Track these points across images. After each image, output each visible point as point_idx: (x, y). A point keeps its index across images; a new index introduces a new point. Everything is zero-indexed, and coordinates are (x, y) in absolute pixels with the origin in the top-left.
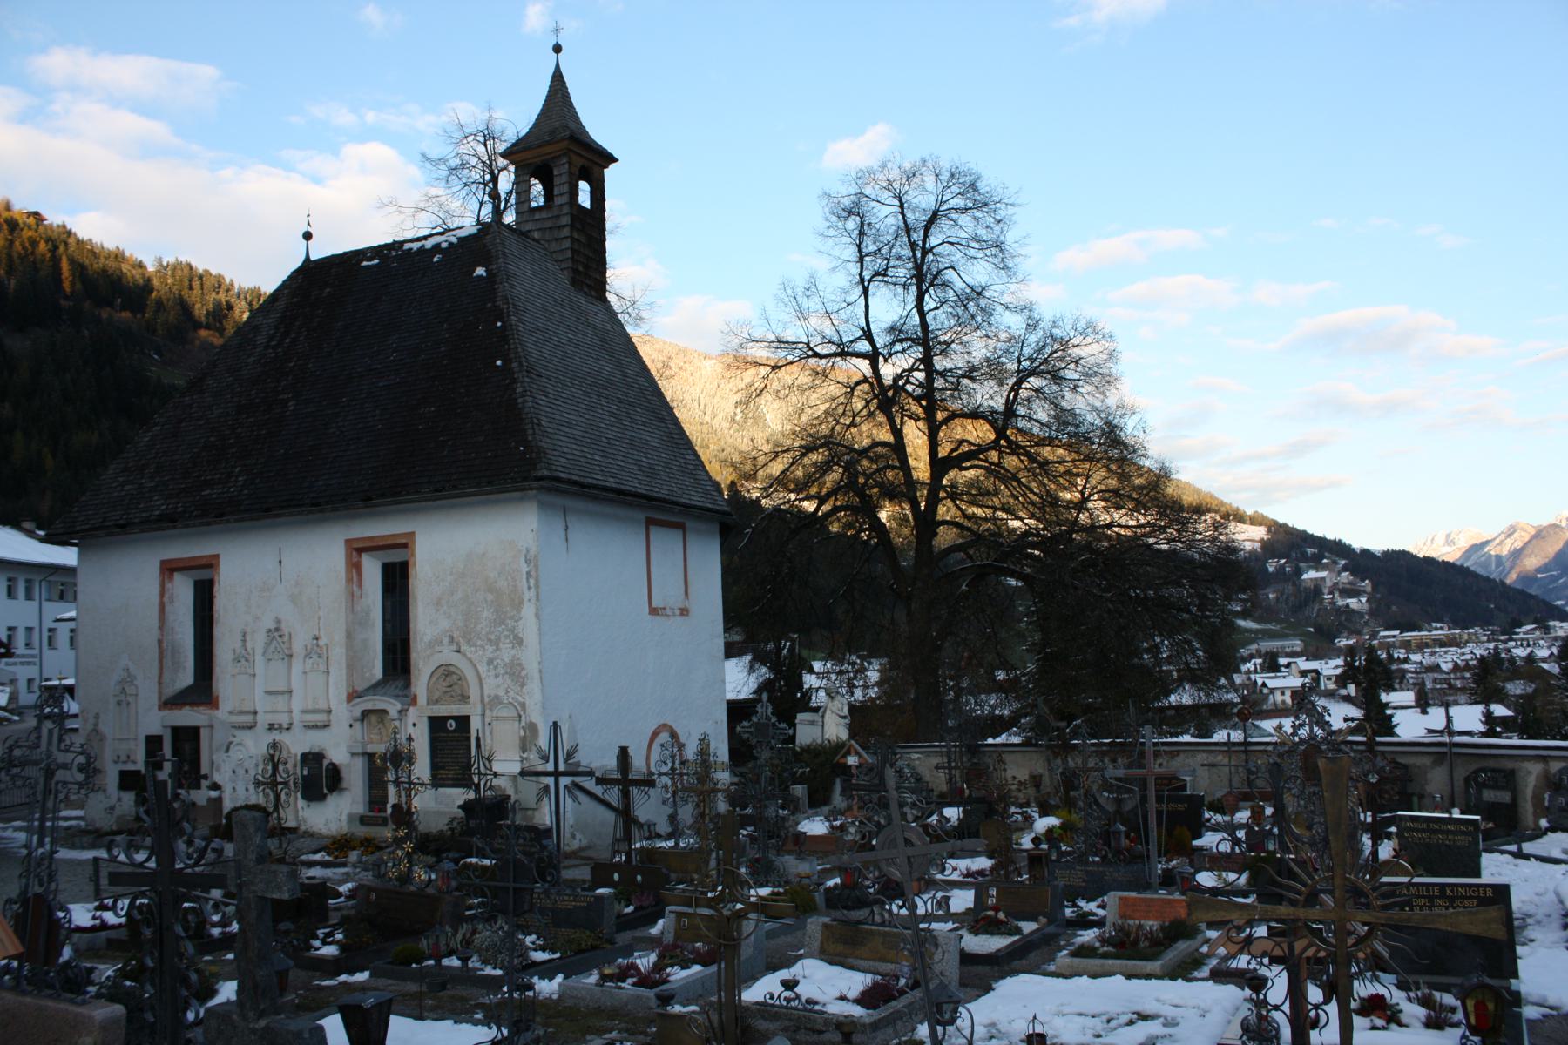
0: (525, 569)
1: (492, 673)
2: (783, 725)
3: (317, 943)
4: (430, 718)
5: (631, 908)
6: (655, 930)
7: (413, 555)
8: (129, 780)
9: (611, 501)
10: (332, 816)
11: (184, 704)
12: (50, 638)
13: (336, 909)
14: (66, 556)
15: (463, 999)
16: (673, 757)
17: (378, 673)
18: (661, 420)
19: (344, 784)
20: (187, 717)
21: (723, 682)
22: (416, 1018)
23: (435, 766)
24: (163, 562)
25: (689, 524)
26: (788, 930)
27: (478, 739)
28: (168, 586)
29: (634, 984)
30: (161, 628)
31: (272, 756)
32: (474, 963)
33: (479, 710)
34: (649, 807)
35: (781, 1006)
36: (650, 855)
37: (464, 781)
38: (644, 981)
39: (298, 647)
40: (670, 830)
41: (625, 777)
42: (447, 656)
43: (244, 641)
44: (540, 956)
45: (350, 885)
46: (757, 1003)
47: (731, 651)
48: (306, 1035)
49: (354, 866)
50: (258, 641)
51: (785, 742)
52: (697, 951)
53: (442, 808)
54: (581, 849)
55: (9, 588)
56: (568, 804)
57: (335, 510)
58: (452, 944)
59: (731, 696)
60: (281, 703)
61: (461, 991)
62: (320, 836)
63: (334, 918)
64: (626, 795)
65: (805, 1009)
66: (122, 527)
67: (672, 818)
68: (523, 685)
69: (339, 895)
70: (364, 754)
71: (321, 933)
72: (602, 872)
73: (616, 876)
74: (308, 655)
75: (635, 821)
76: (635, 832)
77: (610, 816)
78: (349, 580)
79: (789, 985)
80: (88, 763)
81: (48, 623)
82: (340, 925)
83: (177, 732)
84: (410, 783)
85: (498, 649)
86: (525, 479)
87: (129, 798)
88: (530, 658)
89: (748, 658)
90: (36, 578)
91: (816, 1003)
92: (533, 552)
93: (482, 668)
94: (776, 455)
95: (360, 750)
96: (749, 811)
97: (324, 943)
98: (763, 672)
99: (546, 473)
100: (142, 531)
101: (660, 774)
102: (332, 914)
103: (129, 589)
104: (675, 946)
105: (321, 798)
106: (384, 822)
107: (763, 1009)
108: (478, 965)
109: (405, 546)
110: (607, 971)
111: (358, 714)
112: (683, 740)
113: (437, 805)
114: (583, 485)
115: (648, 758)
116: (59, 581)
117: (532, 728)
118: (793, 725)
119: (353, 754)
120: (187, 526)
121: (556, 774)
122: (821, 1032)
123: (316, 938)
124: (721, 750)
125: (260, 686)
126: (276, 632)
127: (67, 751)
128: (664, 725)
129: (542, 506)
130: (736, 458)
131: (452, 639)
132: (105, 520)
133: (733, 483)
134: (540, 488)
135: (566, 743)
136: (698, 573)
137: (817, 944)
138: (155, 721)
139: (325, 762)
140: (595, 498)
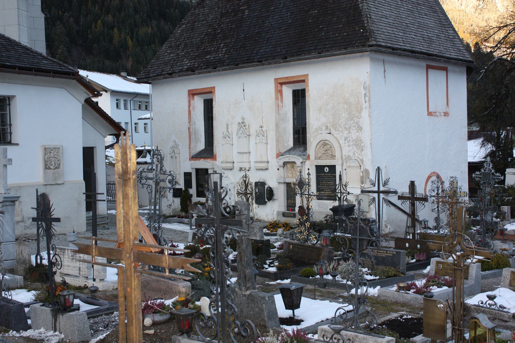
0: (363, 92)
1: (347, 144)
2: (498, 174)
3: (266, 266)
4: (316, 166)
5: (414, 260)
6: (425, 271)
7: (307, 86)
8: (177, 193)
9: (408, 56)
10: (269, 212)
11: (201, 158)
12: (135, 127)
13: (273, 253)
14: (144, 88)
15: (333, 293)
16: (438, 188)
17: (291, 144)
18: (435, 12)
19: (275, 197)
20: (202, 164)
21: (467, 151)
22: (312, 299)
23: (318, 190)
24: (189, 91)
25: (450, 68)
26: (494, 276)
27: (340, 176)
28: (192, 102)
29: (414, 293)
30: (189, 122)
31: (245, 181)
32: (338, 278)
33: (340, 162)
34: (425, 212)
35: (487, 308)
36: (425, 237)
37: (333, 198)
38: (419, 291)
39: (253, 131)
40: (435, 224)
41: (413, 197)
42: (325, 136)
43: (228, 128)
44: (369, 277)
45: (279, 243)
46: (475, 305)
47: (471, 136)
48: (267, 299)
49: (280, 236)
50: (234, 129)
51: (499, 183)
52: (446, 280)
53: (322, 210)
54: (390, 233)
55: (117, 104)
56: (385, 208)
57: (270, 64)
58: (328, 269)
59: (471, 160)
60: (245, 157)
61: (332, 290)
62: (264, 222)
63: (273, 257)
64: (413, 205)
65: (499, 310)
66: (170, 74)
67: (437, 219)
68: (362, 150)
69: (275, 247)
70: (284, 183)
71: (268, 262)
72: (400, 242)
73: (407, 245)
74: (258, 135)
75: (418, 220)
76: (417, 225)
77: (405, 217)
78: (277, 98)
79: (491, 298)
80: (173, 180)
81: (135, 120)
82: (277, 259)
83: (197, 170)
84: (309, 195)
85: (350, 132)
86: (364, 46)
87: (178, 201)
88: (366, 137)
89: (480, 140)
90: (129, 99)
91: (505, 308)
92: (367, 84)
93: (342, 142)
94: (500, 28)
95: (283, 181)
96: (478, 218)
97: (270, 266)
98: (490, 147)
99: (374, 43)
100: (179, 76)
101: (431, 196)
102: (271, 255)
103: (173, 104)
104: (435, 277)
105: (265, 203)
106: (294, 216)
107: (478, 308)
108: (340, 279)
109: (303, 81)
110: (402, 285)
111: (282, 164)
112: (443, 180)
113: (321, 209)
114: (393, 49)
115: (425, 189)
116: (142, 102)
117: (367, 172)
118: (503, 174)
119: (279, 183)
120: (200, 73)
121: (379, 192)
122: (506, 321)
123: (266, 264)
124: (464, 186)
125: (235, 149)
126: (242, 124)
127: (164, 174)
128: (434, 173)
129: (372, 59)
130: (477, 30)
131: (327, 127)
132: (163, 71)
133: (477, 44)
134: (371, 51)
135: (383, 178)
136: (454, 92)
137: (508, 281)
138: (190, 166)
139: (266, 187)
140: (400, 55)
